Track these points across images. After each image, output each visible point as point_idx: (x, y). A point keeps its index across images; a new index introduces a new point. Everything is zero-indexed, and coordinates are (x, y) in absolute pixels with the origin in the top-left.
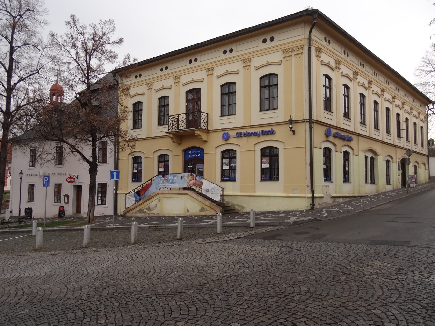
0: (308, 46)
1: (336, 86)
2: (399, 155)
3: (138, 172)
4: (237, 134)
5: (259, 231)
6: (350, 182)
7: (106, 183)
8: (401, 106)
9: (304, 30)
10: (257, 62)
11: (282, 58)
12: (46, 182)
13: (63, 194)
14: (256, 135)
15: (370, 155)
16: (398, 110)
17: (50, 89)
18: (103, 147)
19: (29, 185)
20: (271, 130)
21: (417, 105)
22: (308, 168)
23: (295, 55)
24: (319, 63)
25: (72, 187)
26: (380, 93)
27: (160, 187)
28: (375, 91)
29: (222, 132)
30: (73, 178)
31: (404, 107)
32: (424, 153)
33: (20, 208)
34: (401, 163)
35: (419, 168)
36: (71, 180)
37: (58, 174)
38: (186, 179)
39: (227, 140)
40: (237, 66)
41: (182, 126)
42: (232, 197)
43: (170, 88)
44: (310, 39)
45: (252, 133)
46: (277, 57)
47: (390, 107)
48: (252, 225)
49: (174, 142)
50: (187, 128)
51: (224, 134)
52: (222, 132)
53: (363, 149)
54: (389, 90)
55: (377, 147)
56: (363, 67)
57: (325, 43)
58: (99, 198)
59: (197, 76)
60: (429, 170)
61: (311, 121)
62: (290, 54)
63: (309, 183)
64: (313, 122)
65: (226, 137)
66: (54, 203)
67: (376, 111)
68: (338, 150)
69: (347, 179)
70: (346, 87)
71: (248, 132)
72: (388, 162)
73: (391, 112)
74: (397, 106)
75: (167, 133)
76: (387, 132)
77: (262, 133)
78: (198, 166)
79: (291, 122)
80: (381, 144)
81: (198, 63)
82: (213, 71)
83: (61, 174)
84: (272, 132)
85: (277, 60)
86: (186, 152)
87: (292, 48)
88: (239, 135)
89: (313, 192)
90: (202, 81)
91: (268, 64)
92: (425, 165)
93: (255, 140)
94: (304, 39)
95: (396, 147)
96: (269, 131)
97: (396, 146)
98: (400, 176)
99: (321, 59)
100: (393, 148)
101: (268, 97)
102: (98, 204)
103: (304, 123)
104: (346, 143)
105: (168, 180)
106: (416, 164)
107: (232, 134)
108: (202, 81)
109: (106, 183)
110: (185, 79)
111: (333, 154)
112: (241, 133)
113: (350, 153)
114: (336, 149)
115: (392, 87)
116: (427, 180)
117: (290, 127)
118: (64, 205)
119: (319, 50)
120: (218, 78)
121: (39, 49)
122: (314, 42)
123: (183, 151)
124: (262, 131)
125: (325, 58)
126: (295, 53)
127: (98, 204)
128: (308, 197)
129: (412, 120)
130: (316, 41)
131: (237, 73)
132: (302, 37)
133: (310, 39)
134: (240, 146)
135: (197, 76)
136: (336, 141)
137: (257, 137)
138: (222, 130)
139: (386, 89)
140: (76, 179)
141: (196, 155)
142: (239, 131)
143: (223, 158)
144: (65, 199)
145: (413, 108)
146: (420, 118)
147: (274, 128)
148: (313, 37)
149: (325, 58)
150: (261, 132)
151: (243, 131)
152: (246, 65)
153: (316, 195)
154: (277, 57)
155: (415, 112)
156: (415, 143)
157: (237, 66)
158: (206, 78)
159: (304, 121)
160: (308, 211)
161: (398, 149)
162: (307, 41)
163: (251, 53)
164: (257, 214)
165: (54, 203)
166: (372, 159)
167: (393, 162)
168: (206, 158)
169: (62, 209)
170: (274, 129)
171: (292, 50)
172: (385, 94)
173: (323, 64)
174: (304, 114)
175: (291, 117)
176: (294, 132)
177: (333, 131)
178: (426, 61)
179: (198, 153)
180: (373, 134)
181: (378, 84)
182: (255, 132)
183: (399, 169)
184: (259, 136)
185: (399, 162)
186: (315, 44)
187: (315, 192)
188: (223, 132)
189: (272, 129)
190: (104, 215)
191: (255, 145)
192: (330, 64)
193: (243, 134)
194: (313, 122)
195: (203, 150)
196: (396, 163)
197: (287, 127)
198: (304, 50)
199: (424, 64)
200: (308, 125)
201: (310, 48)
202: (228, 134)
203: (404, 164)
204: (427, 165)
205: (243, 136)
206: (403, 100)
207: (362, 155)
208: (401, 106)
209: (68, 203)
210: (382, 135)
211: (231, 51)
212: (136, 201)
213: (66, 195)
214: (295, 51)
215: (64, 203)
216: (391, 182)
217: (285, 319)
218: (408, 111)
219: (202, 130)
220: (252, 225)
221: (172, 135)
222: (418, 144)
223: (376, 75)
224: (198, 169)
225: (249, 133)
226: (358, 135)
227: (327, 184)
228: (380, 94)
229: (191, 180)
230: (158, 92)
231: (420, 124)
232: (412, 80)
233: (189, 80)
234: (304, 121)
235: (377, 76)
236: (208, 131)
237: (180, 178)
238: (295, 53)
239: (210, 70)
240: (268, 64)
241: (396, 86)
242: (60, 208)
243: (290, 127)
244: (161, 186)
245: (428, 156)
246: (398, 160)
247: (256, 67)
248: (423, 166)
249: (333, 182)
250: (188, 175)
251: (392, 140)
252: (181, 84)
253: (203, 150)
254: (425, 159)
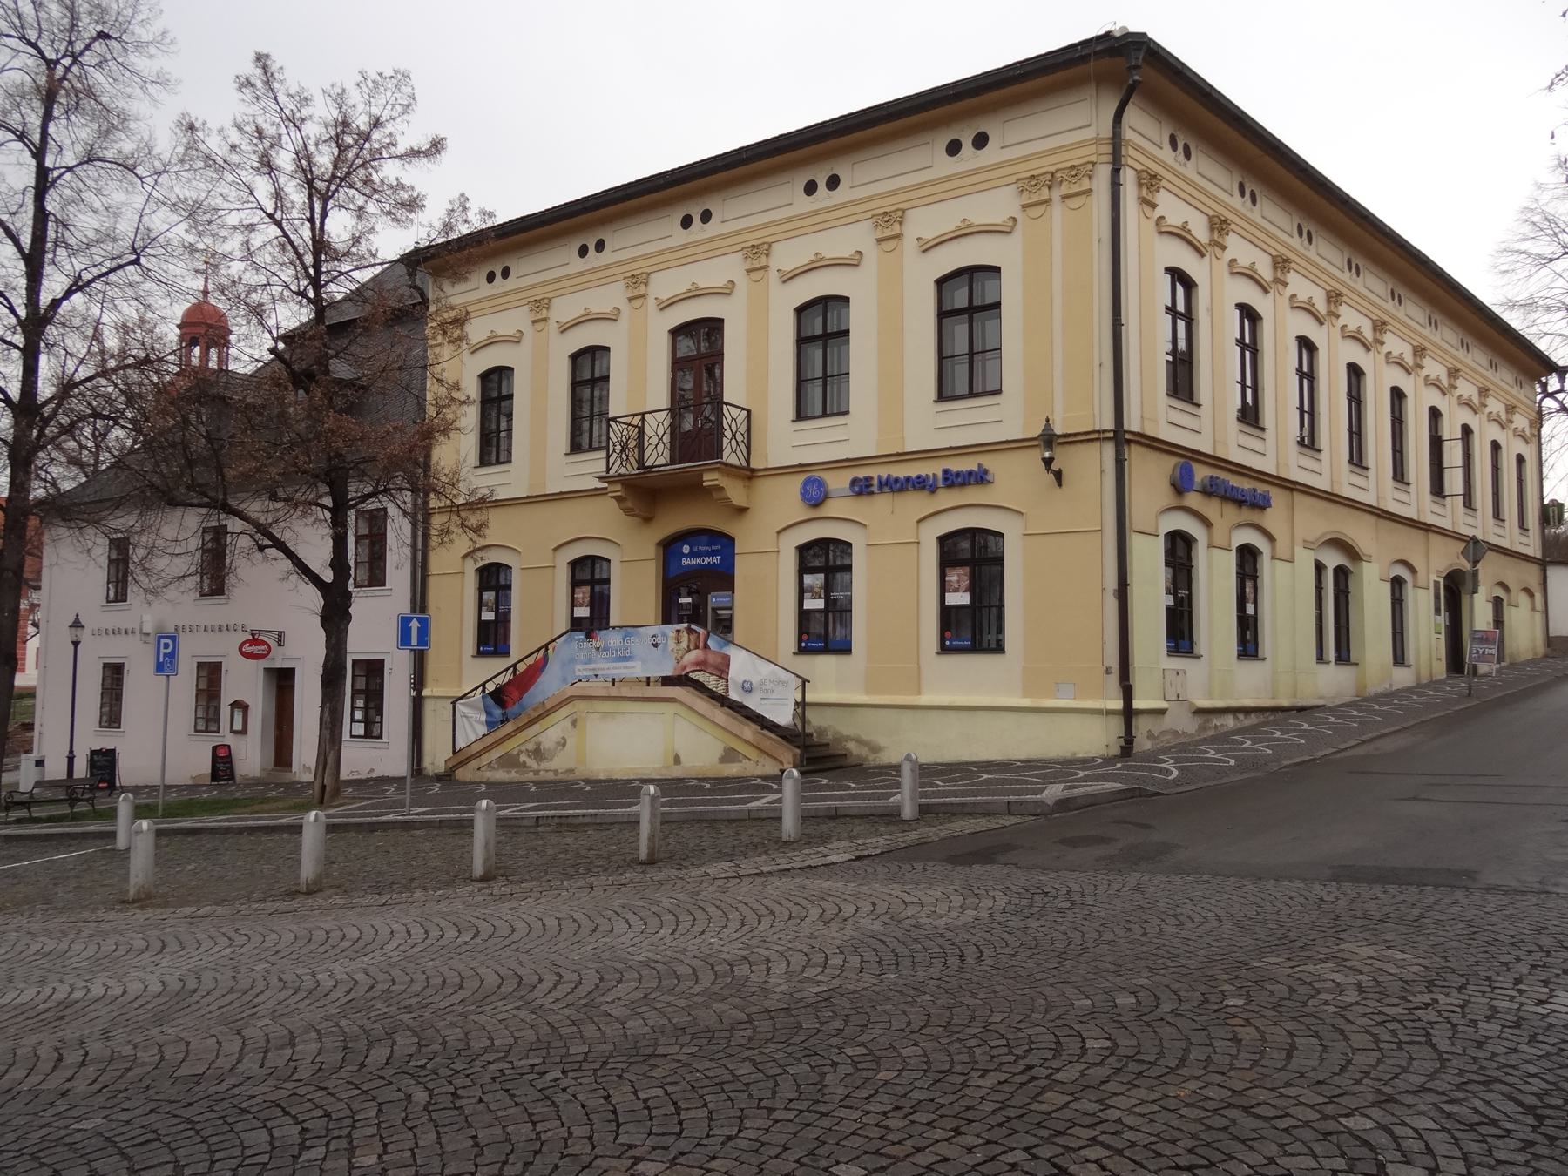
0: (1110, 167)
1: (1211, 310)
2: (1439, 559)
3: (496, 622)
4: (854, 482)
5: (933, 832)
6: (1260, 655)
7: (382, 662)
8: (1445, 381)
9: (1097, 107)
10: (925, 223)
11: (1015, 211)
12: (165, 655)
13: (226, 700)
14: (923, 488)
15: (1332, 560)
16: (1434, 398)
17: (179, 322)
18: (370, 530)
19: (105, 666)
20: (975, 468)
21: (1504, 378)
22: (1112, 605)
23: (1065, 197)
24: (1150, 226)
25: (261, 674)
26: (1368, 334)
27: (578, 673)
28: (1352, 327)
29: (802, 478)
30: (264, 643)
31: (1456, 388)
32: (1530, 552)
33: (71, 751)
34: (1446, 587)
35: (1509, 605)
36: (256, 649)
37: (209, 629)
38: (672, 644)
39: (817, 504)
40: (855, 238)
41: (658, 455)
42: (837, 709)
43: (612, 318)
44: (1117, 141)
45: (908, 479)
46: (999, 205)
47: (1406, 384)
48: (908, 812)
49: (626, 511)
50: (672, 462)
51: (807, 482)
52: (802, 478)
53: (1310, 539)
54: (1403, 324)
55: (1360, 532)
56: (1310, 240)
57: (1173, 154)
58: (358, 715)
59: (711, 274)
60: (1546, 612)
61: (1121, 438)
62: (1045, 193)
63: (1113, 661)
64: (1129, 442)
65: (815, 496)
66: (196, 731)
67: (1355, 399)
68: (1218, 540)
69: (1250, 646)
70: (1248, 314)
71: (895, 475)
72: (1397, 583)
73: (1410, 405)
74: (1431, 383)
75: (601, 479)
76: (1395, 478)
77: (946, 479)
78: (714, 600)
79: (1049, 439)
80: (1372, 519)
81: (714, 228)
82: (767, 255)
83: (220, 629)
84: (980, 478)
85: (998, 218)
86: (669, 547)
87: (1053, 174)
88: (862, 488)
89: (1128, 693)
90: (727, 291)
91: (967, 232)
92: (1531, 594)
93: (917, 504)
94: (1097, 141)
95: (1426, 530)
96: (970, 473)
97: (1427, 528)
98: (1443, 637)
99: (1158, 212)
100: (1418, 535)
101: (966, 351)
102: (352, 736)
103: (1097, 444)
104: (1247, 515)
105: (605, 649)
106: (1500, 593)
107: (838, 482)
108: (727, 291)
109: (382, 662)
110: (665, 285)
111: (1201, 555)
112: (868, 479)
113: (1261, 553)
114: (1210, 536)
115: (1412, 312)
116: (1541, 648)
117: (1044, 460)
118: (229, 739)
119: (1149, 181)
120: (784, 282)
121: (140, 178)
122: (1131, 152)
123: (658, 544)
124: (946, 472)
125: (1172, 209)
126: (1064, 190)
127: (352, 736)
128: (1110, 712)
129: (1485, 434)
130: (1138, 149)
131: (853, 263)
132: (1089, 134)
133: (1117, 141)
134: (865, 525)
135: (711, 274)
136: (1211, 508)
137: (926, 493)
138: (801, 468)
139: (1392, 321)
140: (273, 644)
141: (708, 560)
142: (861, 473)
143: (803, 569)
144: (236, 717)
145: (1487, 390)
146: (1514, 426)
147: (988, 462)
148: (1128, 135)
149: (1172, 209)
150: (940, 474)
151: (875, 472)
152: (888, 233)
153: (1138, 704)
154: (999, 205)
155: (1495, 406)
156: (1497, 514)
157: (855, 238)
158: (742, 282)
159: (1096, 436)
160: (1108, 761)
161: (1434, 538)
162: (1108, 149)
163: (903, 190)
164: (927, 771)
165: (196, 731)
166: (1341, 573)
167: (1415, 586)
168: (743, 569)
169: (222, 753)
170: (986, 465)
171: (1053, 180)
172: (1389, 338)
173: (1166, 231)
174: (1097, 412)
175: (1048, 420)
176: (1058, 476)
177: (1201, 473)
178: (1536, 218)
179: (712, 554)
180: (1346, 483)
181: (1363, 302)
182: (919, 477)
183: (1437, 611)
184: (933, 490)
185: (1437, 584)
186: (1134, 159)
187: (1137, 692)
188: (803, 477)
189: (980, 466)
190: (374, 776)
191: (919, 521)
192: (1189, 232)
193: (875, 482)
194: (1129, 442)
195: (730, 541)
196: (1428, 589)
197: (1034, 458)
198: (1095, 182)
199: (1527, 229)
200: (1109, 450)
201: (1116, 172)
202: (821, 484)
203: (1455, 590)
204: (1538, 596)
205: (875, 489)
206: (1451, 360)
207: (1306, 561)
208: (1445, 381)
209: (244, 731)
210: (1377, 487)
211: (833, 182)
212: (490, 725)
213: (237, 705)
214: (1065, 183)
215: (232, 731)
216: (1411, 655)
217: (1026, 1150)
218: (1470, 400)
219: (729, 470)
220: (908, 812)
221: (618, 487)
222: (1506, 518)
223: (1354, 270)
224: (714, 610)
225: (897, 480)
226: (1292, 487)
227: (1178, 663)
228: (1370, 339)
230: (569, 332)
231: (1513, 447)
232: (1486, 289)
233: (682, 288)
234: (1096, 436)
235: (1358, 274)
236: (749, 474)
237: (649, 642)
238: (1064, 190)
239: (757, 253)
240: (967, 232)
241: (1428, 312)
242: (215, 749)
243: (1044, 460)
244: (581, 670)
245: (1543, 564)
246: (1433, 577)
247: (921, 242)
248: (1523, 599)
249: (1199, 657)
250: (678, 631)
251: (1414, 503)
252: (651, 302)
253: (731, 540)
254: (1531, 575)
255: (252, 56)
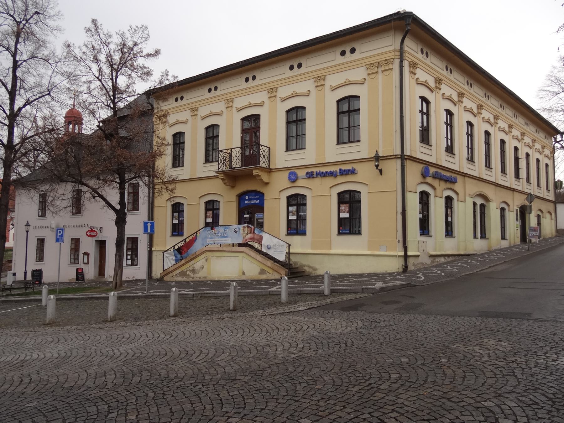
0: (399, 60)
1: (435, 111)
2: (518, 201)
3: (178, 224)
4: (307, 173)
5: (336, 299)
6: (453, 236)
7: (137, 238)
8: (520, 137)
9: (394, 38)
10: (333, 80)
11: (365, 76)
12: (59, 236)
13: (81, 252)
14: (332, 176)
15: (479, 201)
16: (516, 143)
17: (64, 116)
18: (133, 191)
19: (38, 239)
20: (351, 168)
21: (541, 136)
22: (400, 218)
23: (383, 71)
24: (414, 81)
25: (94, 242)
26: (492, 120)
27: (208, 242)
28: (486, 118)
29: (288, 172)
30: (95, 231)
31: (524, 139)
32: (550, 198)
33: (26, 270)
34: (520, 211)
35: (543, 218)
36: (92, 234)
37: (75, 226)
38: (242, 232)
39: (294, 181)
40: (307, 85)
41: (237, 164)
42: (301, 255)
43: (220, 114)
44: (402, 51)
45: (327, 172)
46: (359, 74)
47: (506, 138)
48: (327, 292)
49: (225, 184)
50: (242, 166)
51: (290, 173)
52: (288, 172)
53: (471, 194)
54: (505, 116)
55: (489, 191)
56: (471, 86)
57: (422, 55)
58: (129, 257)
59: (256, 99)
60: (556, 220)
61: (403, 158)
62: (376, 70)
63: (400, 238)
64: (406, 159)
65: (293, 178)
66: (71, 263)
67: (488, 143)
68: (438, 194)
69: (450, 233)
70: (449, 113)
71: (322, 171)
72: (503, 210)
73: (507, 146)
74: (515, 138)
75: (216, 172)
76: (502, 172)
77: (340, 172)
78: (257, 216)
79: (377, 158)
80: (494, 187)
81: (257, 82)
82: (276, 92)
83: (79, 226)
84: (352, 172)
85: (359, 78)
86: (241, 197)
87: (379, 63)
88: (310, 176)
89: (406, 249)
90: (261, 105)
91: (348, 84)
92: (551, 214)
93: (330, 181)
94: (395, 51)
95: (513, 191)
96: (349, 170)
97: (513, 190)
98: (519, 229)
99: (417, 76)
100: (510, 192)
101: (348, 126)
102: (127, 265)
103: (395, 160)
104: (449, 185)
105: (218, 234)
106: (540, 213)
107: (301, 173)
108: (261, 105)
109: (137, 238)
110: (239, 102)
111: (432, 200)
112: (312, 172)
113: (454, 199)
114: (435, 193)
115: (508, 112)
116: (554, 233)
117: (376, 165)
118: (82, 266)
119: (413, 65)
120: (282, 101)
121: (51, 64)
122: (407, 55)
123: (237, 196)
124: (340, 170)
125: (422, 75)
126: (383, 68)
127: (127, 265)
128: (399, 256)
129: (534, 156)
130: (409, 53)
131: (307, 94)
132: (392, 48)
133: (402, 51)
134: (311, 189)
135: (256, 99)
136: (436, 183)
137: (333, 177)
138: (288, 168)
139: (501, 116)
140: (98, 232)
141: (255, 201)
142: (310, 170)
143: (289, 205)
144: (85, 258)
145: (535, 140)
146: (544, 153)
147: (356, 166)
148: (406, 48)
149: (422, 75)
150: (338, 171)
151: (315, 170)
152: (319, 84)
153: (409, 253)
154: (359, 74)
155: (538, 146)
156: (538, 185)
157: (307, 85)
158: (267, 101)
159: (394, 157)
160: (399, 274)
161: (516, 194)
162: (398, 53)
163: (325, 68)
164: (333, 277)
165: (71, 263)
166: (482, 206)
167: (509, 211)
168: (267, 205)
169: (80, 271)
170: (355, 167)
171: (379, 65)
172: (499, 122)
173: (419, 83)
174: (394, 148)
175: (377, 151)
176: (381, 171)
177: (432, 170)
178: (553, 79)
179: (256, 199)
180: (484, 174)
181: (490, 109)
182: (330, 172)
183: (517, 220)
184: (336, 176)
185: (517, 210)
186: (408, 57)
187: (409, 249)
188: (289, 172)
189: (352, 167)
190: (135, 279)
191: (331, 188)
192: (428, 83)
193: (315, 173)
194: (406, 159)
195: (263, 194)
196: (514, 212)
197: (372, 165)
198: (394, 65)
199: (549, 82)
200: (399, 162)
201: (401, 62)
202: (295, 174)
203: (523, 212)
204: (553, 214)
205: (315, 176)
206: (522, 129)
207: (470, 202)
208: (520, 137)
209: (88, 263)
210: (495, 175)
211: (300, 66)
212: (176, 261)
213: (85, 253)
214: (383, 66)
215: (83, 263)
216: (508, 236)
218: (529, 144)
219: (262, 169)
220: (327, 292)
221: (222, 175)
222: (542, 186)
223: (487, 97)
224: (257, 219)
225: (323, 173)
226: (465, 175)
227: (424, 238)
228: (493, 122)
229: (248, 234)
230: (205, 120)
231: (544, 161)
232: (535, 104)
233: (245, 104)
234: (394, 157)
235: (488, 99)
236: (269, 171)
237: (233, 231)
238: (383, 68)
239: (272, 91)
240: (348, 84)
241: (514, 112)
242: (77, 269)
243: (376, 165)
244: (209, 241)
245: (555, 203)
246: (516, 208)
247: (331, 87)
248: (548, 215)
249: (431, 236)
250: (244, 227)
251: (509, 181)
252: (234, 109)
253: (263, 194)
254: (551, 207)
255: (91, 20)
